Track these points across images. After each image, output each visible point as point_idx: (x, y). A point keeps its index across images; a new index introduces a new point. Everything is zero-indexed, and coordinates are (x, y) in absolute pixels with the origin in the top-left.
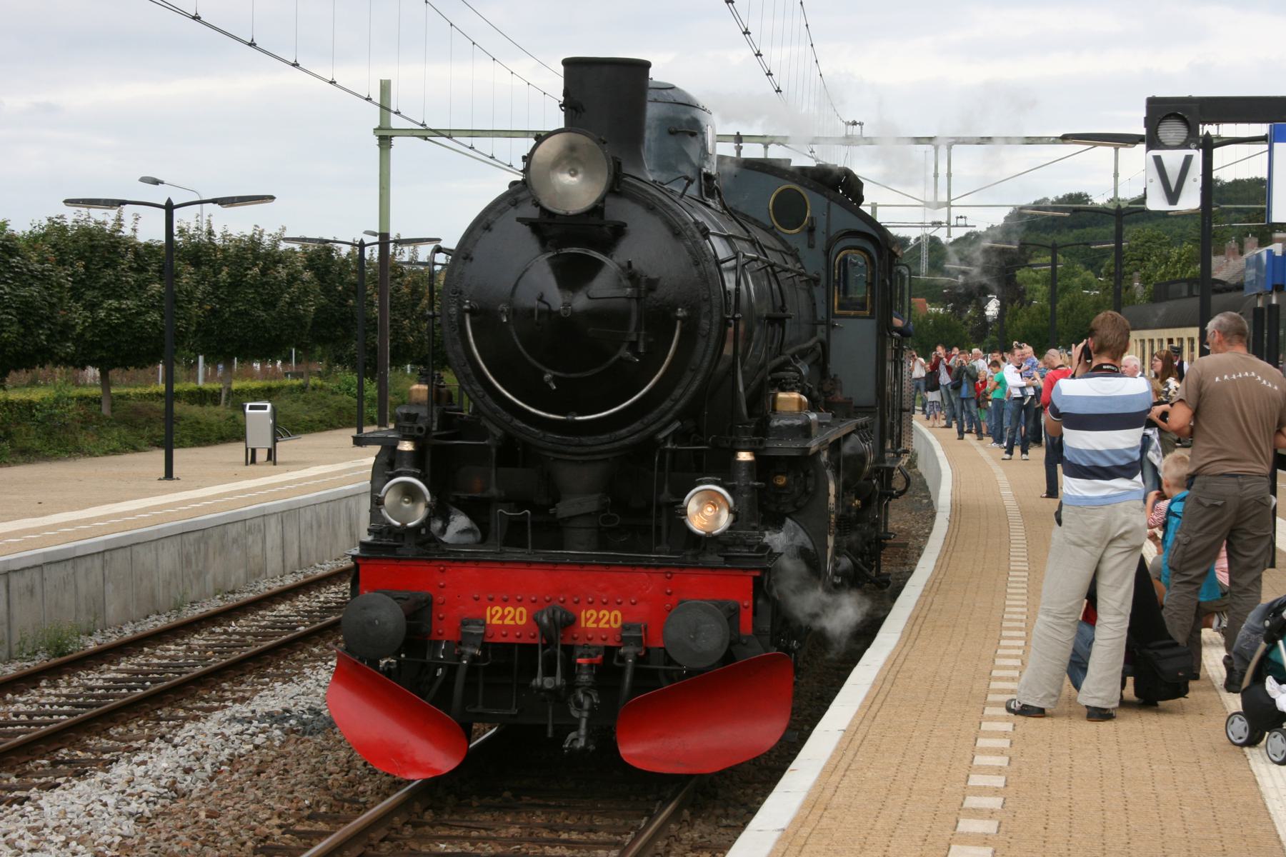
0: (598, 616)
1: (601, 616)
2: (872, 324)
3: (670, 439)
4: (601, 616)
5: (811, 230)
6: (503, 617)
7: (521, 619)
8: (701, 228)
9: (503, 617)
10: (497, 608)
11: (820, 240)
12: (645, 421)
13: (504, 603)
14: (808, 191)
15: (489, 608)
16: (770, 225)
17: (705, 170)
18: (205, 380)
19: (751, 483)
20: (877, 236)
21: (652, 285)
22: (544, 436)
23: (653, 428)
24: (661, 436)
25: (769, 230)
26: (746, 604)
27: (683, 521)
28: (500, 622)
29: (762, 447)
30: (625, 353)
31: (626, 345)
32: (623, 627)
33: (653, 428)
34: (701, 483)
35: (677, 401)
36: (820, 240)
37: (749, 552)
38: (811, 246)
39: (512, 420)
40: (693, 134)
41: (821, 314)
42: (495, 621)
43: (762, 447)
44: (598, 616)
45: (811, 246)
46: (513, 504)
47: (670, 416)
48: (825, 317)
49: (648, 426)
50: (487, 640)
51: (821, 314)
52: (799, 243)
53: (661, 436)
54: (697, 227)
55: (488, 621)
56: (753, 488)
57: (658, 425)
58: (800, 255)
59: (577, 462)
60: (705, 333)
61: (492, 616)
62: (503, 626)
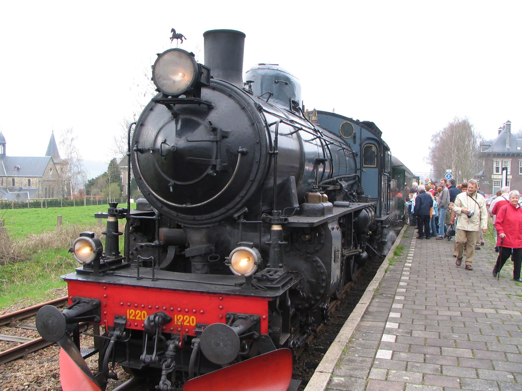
0: (135, 313)
1: (185, 319)
2: (377, 170)
3: (242, 217)
4: (185, 319)
5: (355, 137)
6: (135, 316)
7: (193, 322)
8: (257, 106)
9: (135, 316)
10: (132, 310)
11: (358, 141)
12: (227, 207)
13: (136, 308)
14: (354, 124)
15: (176, 315)
16: (340, 135)
17: (292, 99)
18: (349, 194)
19: (279, 242)
20: (378, 140)
21: (225, 136)
22: (177, 215)
23: (231, 211)
24: (236, 216)
25: (340, 137)
26: (264, 317)
27: (228, 267)
28: (134, 318)
29: (286, 222)
30: (210, 171)
31: (210, 167)
32: (196, 326)
33: (231, 211)
34: (240, 245)
35: (243, 198)
36: (358, 141)
37: (271, 285)
38: (355, 143)
39: (162, 207)
40: (286, 84)
41: (358, 166)
42: (131, 317)
43: (286, 222)
44: (135, 313)
45: (355, 143)
46: (177, 247)
47: (240, 205)
48: (360, 167)
49: (229, 210)
50: (128, 327)
51: (358, 166)
52: (350, 141)
53: (236, 216)
54: (256, 106)
55: (128, 318)
56: (280, 245)
57: (234, 210)
58: (351, 146)
59: (193, 228)
60: (257, 160)
61: (130, 315)
62: (135, 321)
